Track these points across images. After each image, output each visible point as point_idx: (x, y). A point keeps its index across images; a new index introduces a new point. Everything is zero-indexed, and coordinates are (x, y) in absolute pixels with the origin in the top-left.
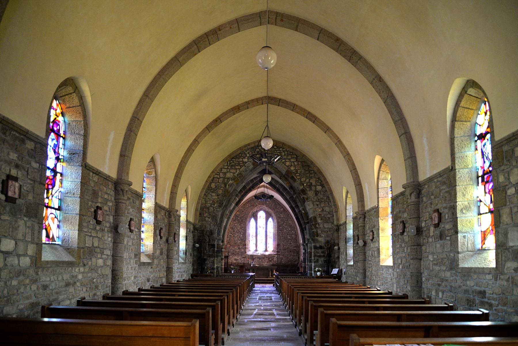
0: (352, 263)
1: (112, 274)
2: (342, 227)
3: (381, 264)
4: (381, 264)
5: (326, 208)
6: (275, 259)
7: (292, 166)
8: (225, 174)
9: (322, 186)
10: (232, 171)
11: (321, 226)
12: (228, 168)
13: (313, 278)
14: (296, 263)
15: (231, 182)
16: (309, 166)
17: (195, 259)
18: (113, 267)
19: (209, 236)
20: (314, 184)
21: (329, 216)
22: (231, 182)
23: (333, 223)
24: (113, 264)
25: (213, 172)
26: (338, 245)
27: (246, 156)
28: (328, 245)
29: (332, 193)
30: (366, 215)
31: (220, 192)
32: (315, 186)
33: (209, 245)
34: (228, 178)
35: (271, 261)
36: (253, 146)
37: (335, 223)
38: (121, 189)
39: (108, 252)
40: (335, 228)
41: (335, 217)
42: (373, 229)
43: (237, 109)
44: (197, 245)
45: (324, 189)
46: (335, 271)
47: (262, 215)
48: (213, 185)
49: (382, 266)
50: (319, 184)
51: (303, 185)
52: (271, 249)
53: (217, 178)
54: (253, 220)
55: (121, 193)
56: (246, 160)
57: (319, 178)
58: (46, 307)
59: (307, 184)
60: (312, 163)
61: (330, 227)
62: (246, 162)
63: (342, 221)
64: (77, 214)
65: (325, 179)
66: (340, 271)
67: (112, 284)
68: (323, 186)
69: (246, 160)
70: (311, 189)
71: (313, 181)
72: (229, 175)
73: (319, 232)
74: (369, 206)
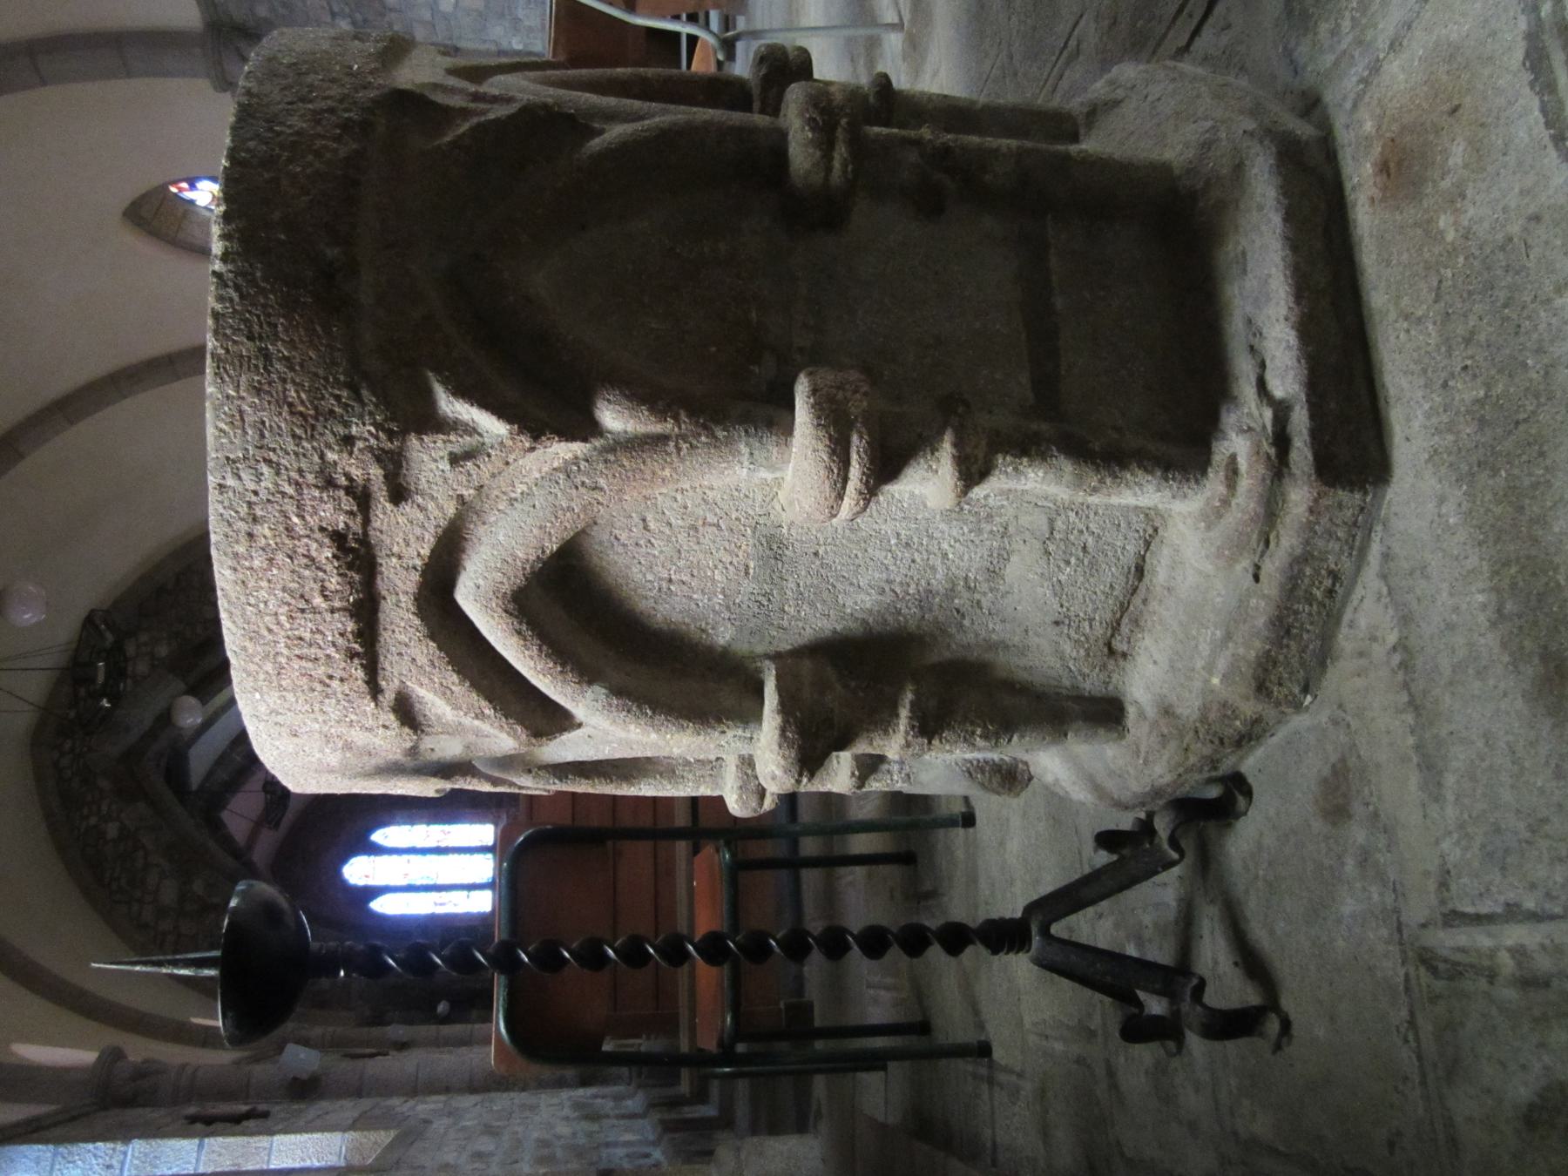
22: (198, 887)
44: (442, 1007)
54: (380, 905)
56: (112, 830)
64: (201, 1146)
69: (112, 830)
72: (169, 893)
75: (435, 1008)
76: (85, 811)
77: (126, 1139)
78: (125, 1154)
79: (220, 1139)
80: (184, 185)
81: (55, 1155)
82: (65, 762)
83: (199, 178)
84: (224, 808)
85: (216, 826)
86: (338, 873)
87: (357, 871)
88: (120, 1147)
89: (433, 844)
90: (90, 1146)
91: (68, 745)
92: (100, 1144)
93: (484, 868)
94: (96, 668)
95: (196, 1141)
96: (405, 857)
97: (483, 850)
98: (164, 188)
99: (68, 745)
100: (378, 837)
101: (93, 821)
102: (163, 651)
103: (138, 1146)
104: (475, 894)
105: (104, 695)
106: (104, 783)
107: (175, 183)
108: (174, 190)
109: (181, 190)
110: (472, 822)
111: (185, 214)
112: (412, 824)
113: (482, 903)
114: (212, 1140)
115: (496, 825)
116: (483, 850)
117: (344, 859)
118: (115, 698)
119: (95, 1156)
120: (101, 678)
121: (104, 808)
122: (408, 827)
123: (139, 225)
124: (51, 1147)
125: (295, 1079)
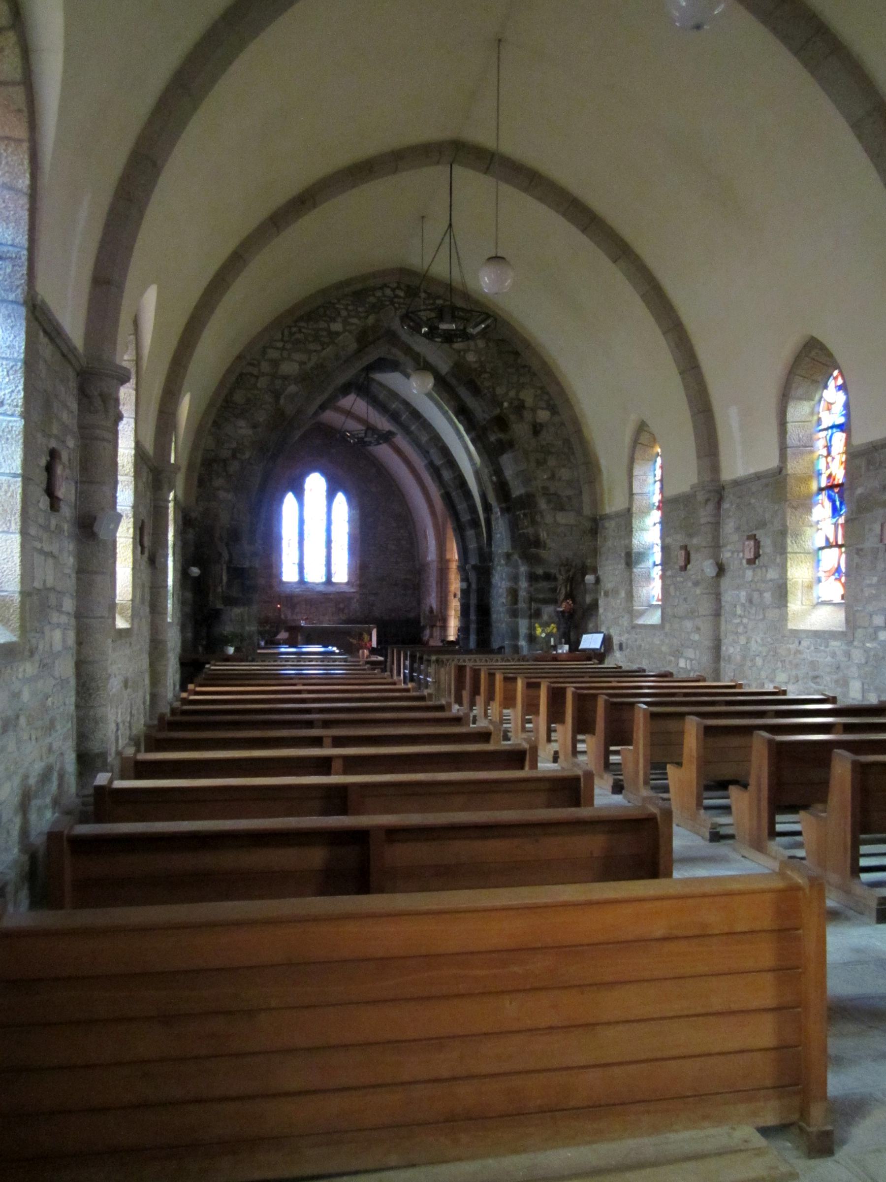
0: (655, 618)
1: (78, 675)
2: (611, 525)
3: (791, 626)
4: (791, 626)
5: (563, 470)
6: (355, 605)
7: (469, 350)
8: (275, 363)
9: (553, 410)
10: (297, 356)
11: (549, 519)
12: (283, 349)
13: (524, 659)
14: (412, 615)
15: (292, 388)
16: (517, 354)
17: (188, 609)
18: (79, 653)
19: (227, 545)
20: (529, 402)
21: (569, 492)
22: (292, 388)
23: (579, 512)
24: (79, 643)
25: (239, 357)
26: (594, 571)
27: (339, 314)
28: (569, 571)
29: (579, 432)
30: (725, 493)
31: (261, 417)
32: (534, 410)
33: (228, 568)
34: (285, 378)
35: (342, 610)
36: (359, 286)
37: (587, 511)
38: (101, 395)
39: (69, 604)
40: (588, 525)
41: (586, 498)
42: (760, 534)
43: (363, 171)
44: (195, 571)
45: (556, 419)
46: (591, 641)
47: (315, 484)
48: (239, 397)
49: (795, 633)
50: (543, 404)
51: (500, 405)
52: (341, 575)
53: (252, 375)
54: (290, 499)
55: (98, 402)
56: (336, 327)
57: (542, 388)
58: (66, 832)
59: (511, 403)
60: (527, 345)
61: (572, 522)
62: (338, 334)
63: (613, 504)
64: (15, 475)
65: (562, 392)
66: (607, 641)
67: (77, 707)
68: (553, 410)
69: (336, 327)
70: (521, 418)
71: (528, 396)
72: (289, 368)
73: (543, 535)
74: (737, 464)
75: (194, 566)
76: (350, 308)
77: (26, 415)
78: (12, 415)
79: (20, 490)
80: (840, 381)
81: (15, 360)
82: (388, 292)
83: (846, 392)
84: (358, 395)
85: (345, 389)
86: (314, 470)
87: (315, 484)
88: (19, 410)
89: (333, 537)
90: (21, 387)
91: (402, 294)
92: (22, 394)
93: (315, 575)
94: (451, 323)
95: (20, 471)
96: (325, 517)
97: (329, 574)
98: (837, 367)
99: (402, 294)
100: (341, 499)
101: (344, 313)
102: (471, 357)
103: (18, 424)
104: (296, 569)
105: (430, 328)
106: (371, 320)
107: (841, 373)
108: (836, 373)
109: (836, 378)
110: (350, 567)
111: (815, 382)
112: (349, 522)
113: (289, 574)
114: (20, 484)
115: (348, 583)
116: (329, 574)
117: (324, 473)
118: (426, 335)
119: (13, 391)
120: (444, 326)
121: (355, 321)
122: (347, 519)
123: (805, 346)
124: (22, 356)
125: (95, 518)
